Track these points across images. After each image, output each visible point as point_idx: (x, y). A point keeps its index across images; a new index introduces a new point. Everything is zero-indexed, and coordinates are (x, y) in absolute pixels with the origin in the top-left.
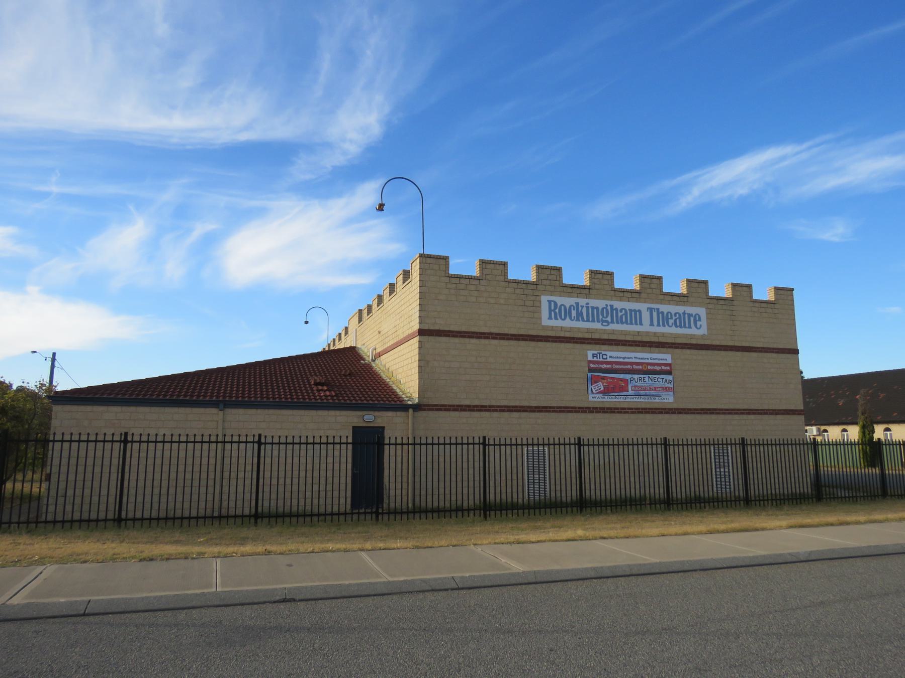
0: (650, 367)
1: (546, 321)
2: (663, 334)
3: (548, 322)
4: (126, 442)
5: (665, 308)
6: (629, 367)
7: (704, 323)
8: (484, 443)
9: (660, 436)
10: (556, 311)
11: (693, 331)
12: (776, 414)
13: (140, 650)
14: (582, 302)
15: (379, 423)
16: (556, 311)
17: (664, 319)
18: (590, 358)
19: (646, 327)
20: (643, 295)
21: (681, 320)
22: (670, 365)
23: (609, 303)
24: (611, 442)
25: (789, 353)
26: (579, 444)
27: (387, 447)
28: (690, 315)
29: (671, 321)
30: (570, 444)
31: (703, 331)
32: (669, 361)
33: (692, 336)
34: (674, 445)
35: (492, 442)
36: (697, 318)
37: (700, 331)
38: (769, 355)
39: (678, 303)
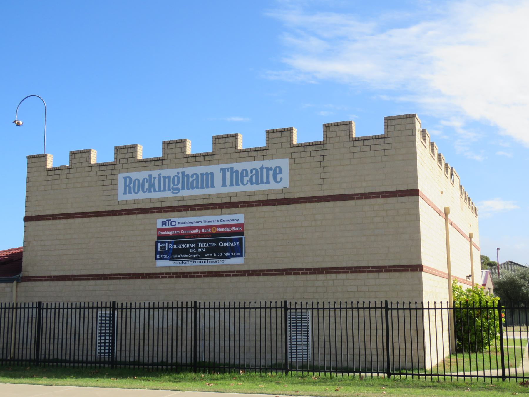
0: (219, 230)
1: (121, 197)
2: (236, 194)
3: (124, 197)
5: (239, 166)
7: (285, 175)
10: (132, 186)
11: (273, 186)
14: (155, 173)
16: (132, 186)
18: (159, 226)
19: (219, 190)
20: (215, 157)
22: (242, 225)
23: (180, 170)
24: (217, 306)
28: (269, 169)
32: (241, 221)
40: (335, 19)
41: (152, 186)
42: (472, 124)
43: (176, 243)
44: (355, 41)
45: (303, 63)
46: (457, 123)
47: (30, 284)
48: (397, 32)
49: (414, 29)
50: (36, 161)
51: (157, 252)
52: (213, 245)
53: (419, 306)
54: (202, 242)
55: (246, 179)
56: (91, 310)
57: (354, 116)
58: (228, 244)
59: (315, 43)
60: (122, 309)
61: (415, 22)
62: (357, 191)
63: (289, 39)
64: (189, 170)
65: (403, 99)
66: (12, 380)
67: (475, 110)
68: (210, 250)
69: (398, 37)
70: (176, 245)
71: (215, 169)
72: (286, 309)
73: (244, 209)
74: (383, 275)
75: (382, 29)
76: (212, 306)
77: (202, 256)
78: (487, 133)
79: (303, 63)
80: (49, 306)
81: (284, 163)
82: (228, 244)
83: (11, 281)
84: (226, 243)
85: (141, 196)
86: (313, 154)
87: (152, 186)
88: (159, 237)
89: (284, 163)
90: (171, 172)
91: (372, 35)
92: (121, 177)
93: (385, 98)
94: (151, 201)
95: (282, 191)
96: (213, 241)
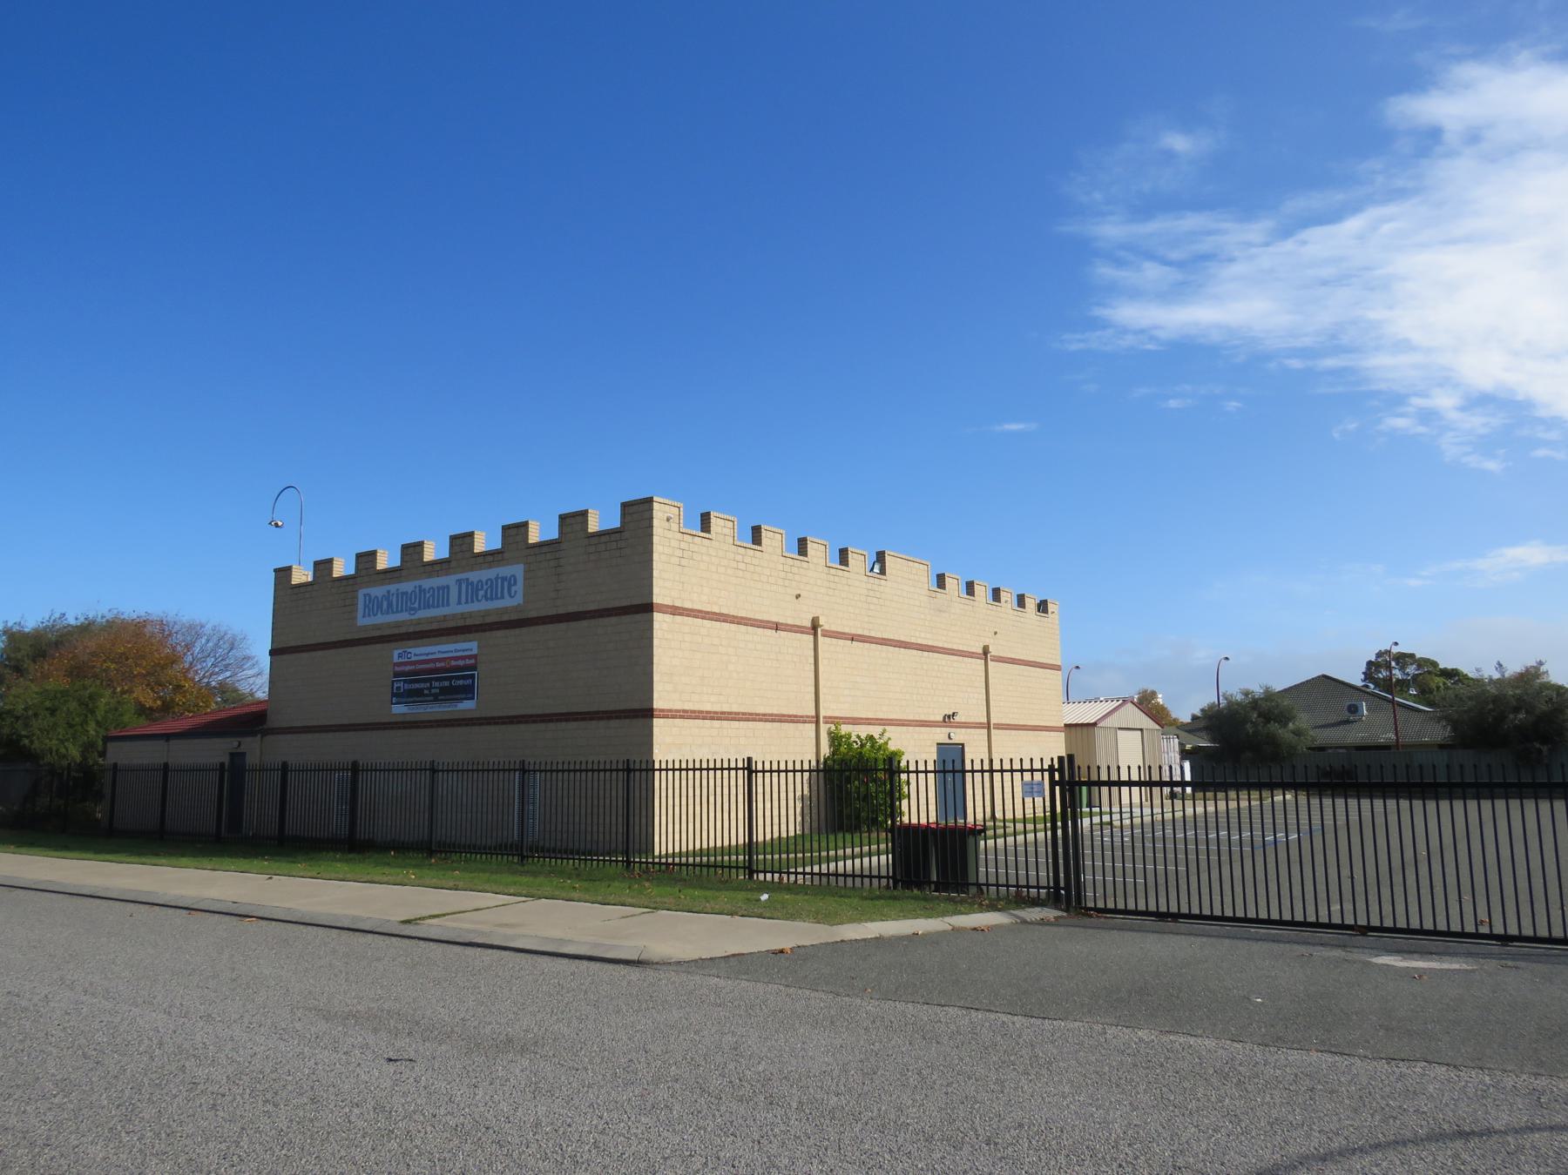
0: (453, 663)
1: (362, 621)
2: (471, 615)
3: (365, 621)
4: (629, 770)
5: (474, 576)
6: (431, 665)
7: (519, 587)
8: (434, 771)
9: (737, 756)
10: (374, 606)
11: (507, 602)
12: (609, 718)
13: (919, 1074)
14: (393, 588)
15: (957, 739)
16: (374, 606)
17: (473, 590)
18: (396, 660)
19: (456, 608)
20: (453, 564)
21: (493, 590)
22: (475, 657)
23: (417, 583)
24: (783, 767)
25: (601, 616)
26: (750, 769)
27: (969, 776)
28: (504, 579)
29: (481, 593)
30: (737, 769)
31: (518, 600)
32: (475, 652)
33: (505, 610)
34: (764, 771)
35: (760, 767)
36: (512, 581)
37: (512, 602)
38: (606, 620)
39: (490, 565)
40: (1191, 222)
41: (390, 605)
42: (1480, 401)
43: (411, 682)
44: (1231, 260)
45: (1129, 314)
46: (1445, 401)
47: (281, 737)
48: (1316, 233)
49: (1353, 224)
50: (283, 574)
51: (393, 695)
52: (446, 684)
53: (958, 767)
54: (437, 679)
55: (481, 593)
56: (783, 775)
57: (1234, 404)
58: (461, 682)
59: (1152, 272)
60: (764, 771)
61: (1354, 208)
62: (592, 607)
63: (1105, 271)
64: (427, 583)
65: (1330, 363)
66: (136, 859)
67: (1484, 369)
68: (443, 690)
69: (1322, 243)
70: (421, 684)
71: (449, 580)
72: (629, 770)
73: (478, 635)
74: (614, 723)
75: (1286, 232)
76: (922, 768)
77: (436, 699)
78: (1512, 418)
79: (1129, 314)
80: (767, 767)
81: (517, 570)
82: (461, 682)
83: (253, 734)
84: (454, 682)
85: (380, 619)
86: (549, 556)
87: (390, 605)
88: (396, 675)
89: (517, 570)
90: (408, 587)
91: (1267, 244)
92: (361, 593)
93: (1295, 364)
94: (389, 625)
95: (516, 609)
96: (445, 679)
